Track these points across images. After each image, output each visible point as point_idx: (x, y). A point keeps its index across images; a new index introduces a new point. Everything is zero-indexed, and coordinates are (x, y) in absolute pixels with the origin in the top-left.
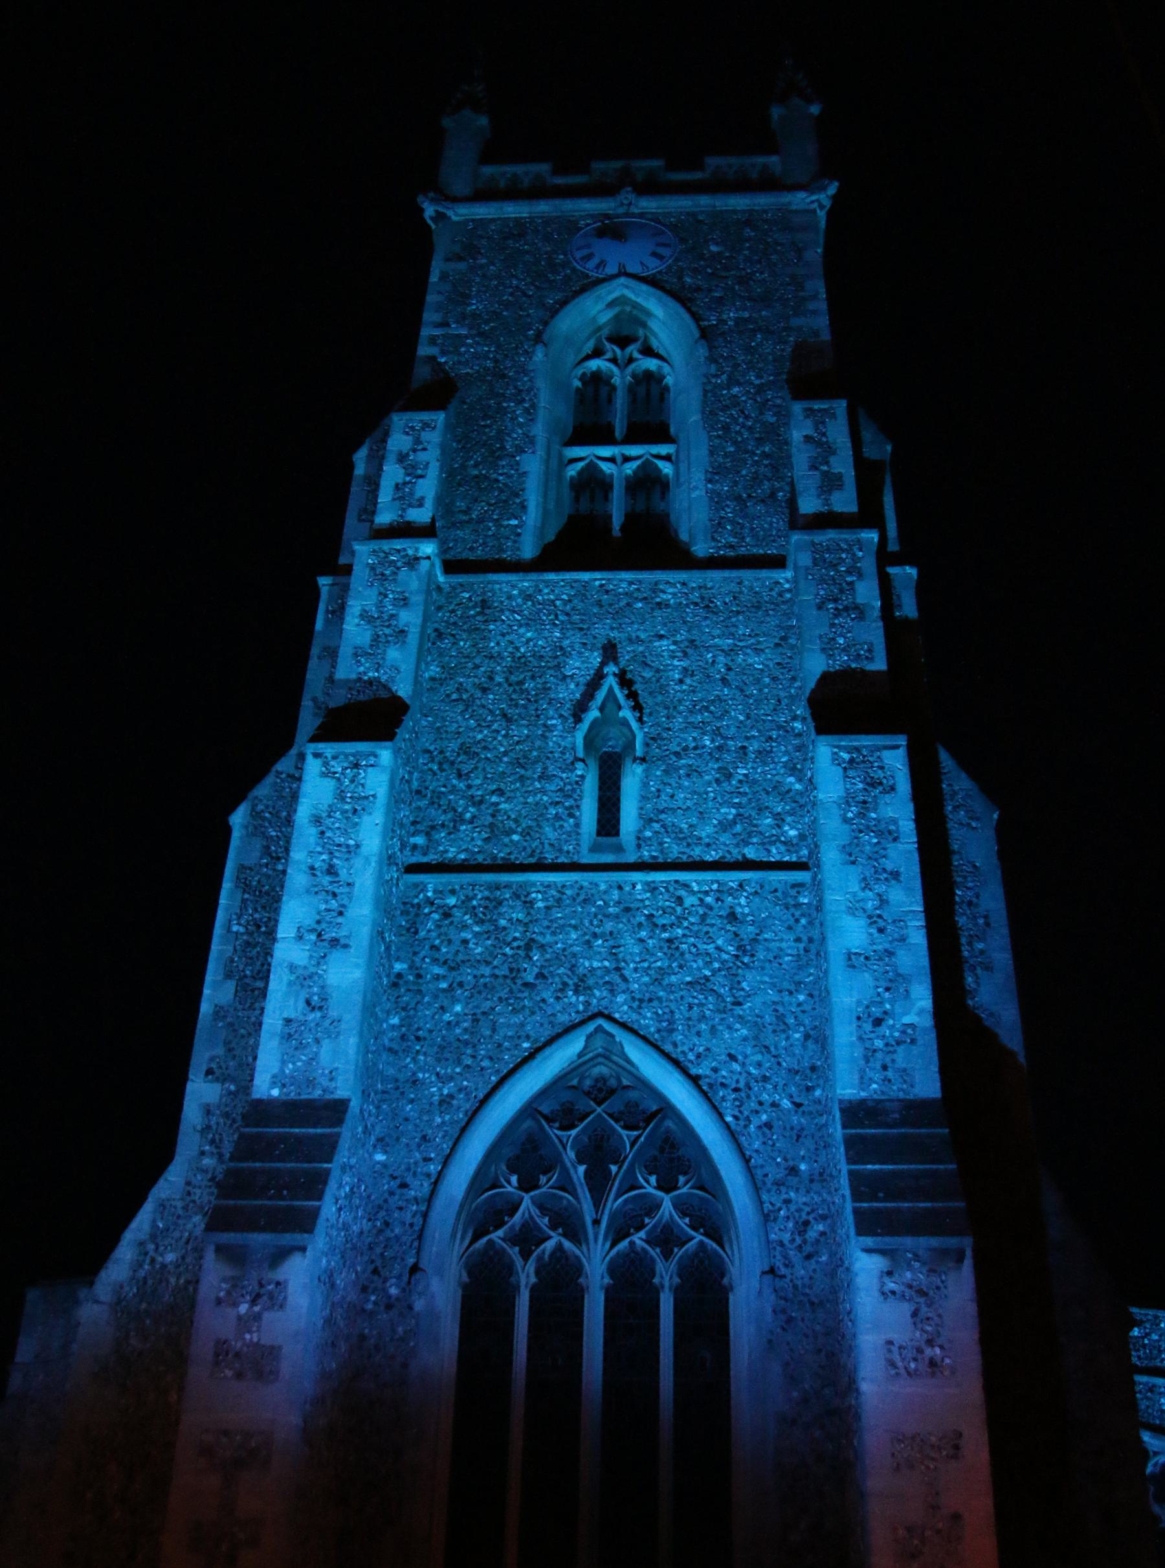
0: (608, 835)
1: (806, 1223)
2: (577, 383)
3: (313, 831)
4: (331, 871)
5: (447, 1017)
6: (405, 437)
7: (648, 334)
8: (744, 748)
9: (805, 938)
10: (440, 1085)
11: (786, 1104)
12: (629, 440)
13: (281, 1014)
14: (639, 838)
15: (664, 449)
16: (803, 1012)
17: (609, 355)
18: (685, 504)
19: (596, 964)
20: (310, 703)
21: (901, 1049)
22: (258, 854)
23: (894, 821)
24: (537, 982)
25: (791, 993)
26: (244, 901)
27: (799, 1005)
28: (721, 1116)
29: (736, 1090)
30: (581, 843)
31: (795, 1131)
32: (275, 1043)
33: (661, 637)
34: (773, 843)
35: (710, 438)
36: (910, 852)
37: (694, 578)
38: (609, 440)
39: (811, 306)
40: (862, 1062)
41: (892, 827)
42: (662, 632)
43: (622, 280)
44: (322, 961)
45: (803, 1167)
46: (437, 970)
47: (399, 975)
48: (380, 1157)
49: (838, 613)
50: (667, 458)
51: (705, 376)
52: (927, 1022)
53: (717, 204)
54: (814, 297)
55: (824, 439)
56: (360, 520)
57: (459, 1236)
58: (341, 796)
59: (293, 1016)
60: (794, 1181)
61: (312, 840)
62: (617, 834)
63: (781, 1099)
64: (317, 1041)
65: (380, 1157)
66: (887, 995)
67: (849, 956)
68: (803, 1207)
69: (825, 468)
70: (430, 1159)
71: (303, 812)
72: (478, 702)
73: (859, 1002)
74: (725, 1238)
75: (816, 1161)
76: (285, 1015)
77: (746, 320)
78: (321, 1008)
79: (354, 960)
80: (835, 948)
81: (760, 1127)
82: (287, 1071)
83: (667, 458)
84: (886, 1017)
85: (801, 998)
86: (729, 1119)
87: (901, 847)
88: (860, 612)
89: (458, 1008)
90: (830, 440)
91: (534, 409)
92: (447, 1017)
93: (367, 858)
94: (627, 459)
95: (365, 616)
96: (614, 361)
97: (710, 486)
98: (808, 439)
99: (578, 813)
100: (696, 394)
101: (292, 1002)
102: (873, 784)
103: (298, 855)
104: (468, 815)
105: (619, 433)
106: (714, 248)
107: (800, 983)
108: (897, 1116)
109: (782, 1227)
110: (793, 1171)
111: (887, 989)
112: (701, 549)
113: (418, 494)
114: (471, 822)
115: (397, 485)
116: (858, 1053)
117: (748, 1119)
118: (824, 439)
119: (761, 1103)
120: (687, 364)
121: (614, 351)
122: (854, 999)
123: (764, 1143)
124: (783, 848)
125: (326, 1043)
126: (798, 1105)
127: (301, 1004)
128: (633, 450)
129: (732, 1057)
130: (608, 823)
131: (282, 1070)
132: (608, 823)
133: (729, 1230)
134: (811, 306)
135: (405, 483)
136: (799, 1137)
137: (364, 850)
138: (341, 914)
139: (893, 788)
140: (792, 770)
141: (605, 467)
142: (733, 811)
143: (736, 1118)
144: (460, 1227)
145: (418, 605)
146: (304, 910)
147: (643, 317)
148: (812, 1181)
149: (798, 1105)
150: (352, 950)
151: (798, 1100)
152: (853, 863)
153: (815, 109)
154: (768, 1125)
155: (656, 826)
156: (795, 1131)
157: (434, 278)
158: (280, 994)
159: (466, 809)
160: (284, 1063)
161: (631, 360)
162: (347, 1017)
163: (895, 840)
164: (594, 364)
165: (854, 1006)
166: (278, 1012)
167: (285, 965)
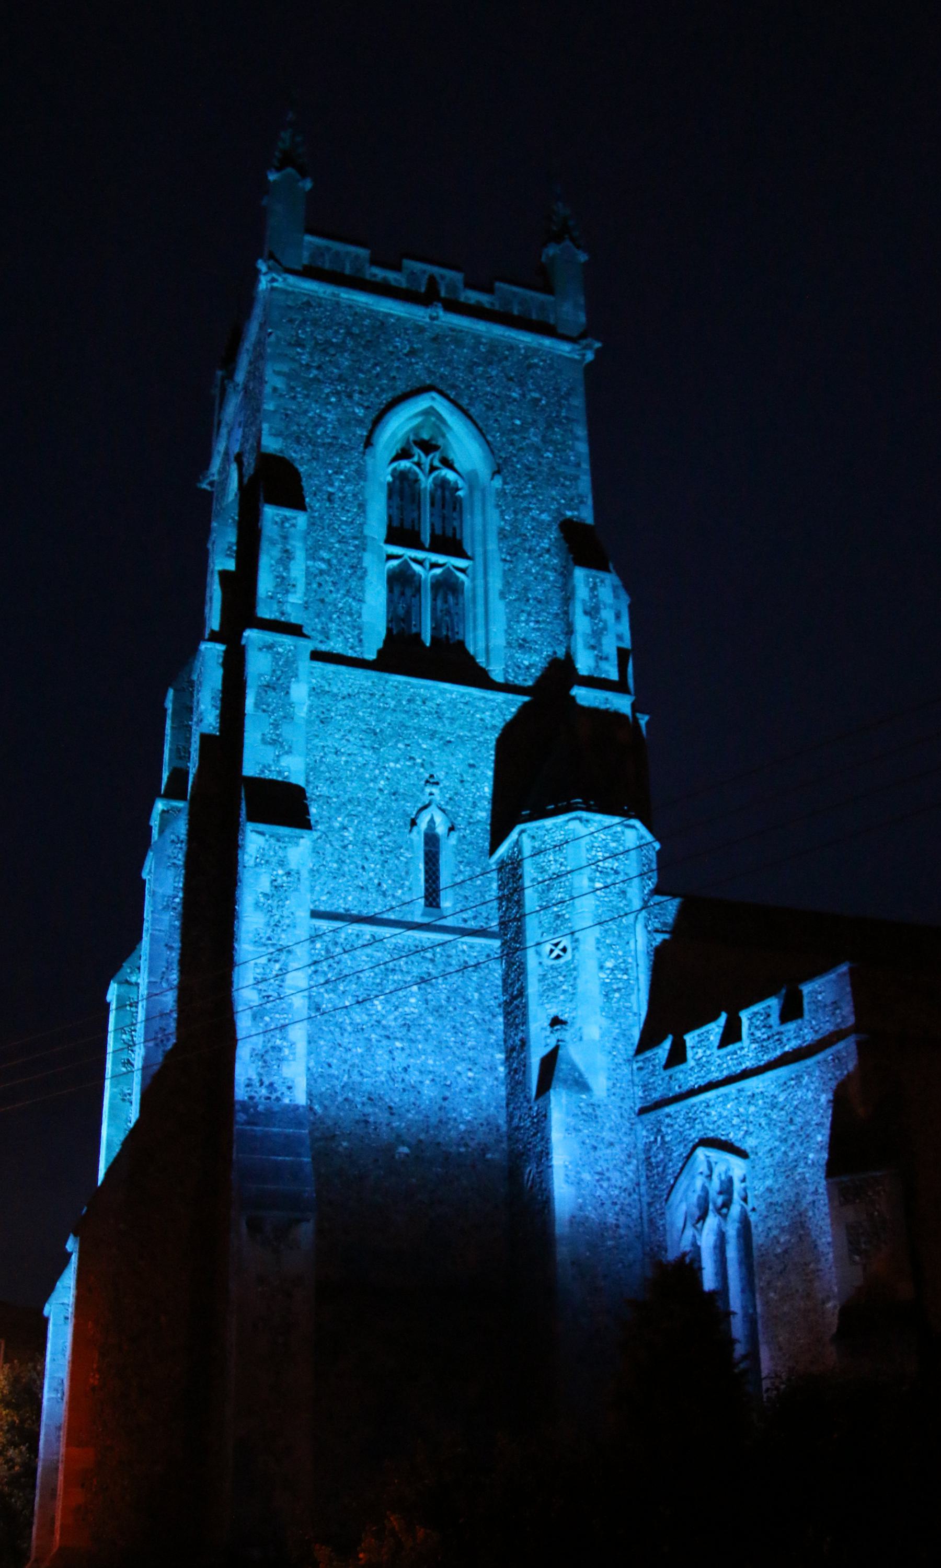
2: (390, 479)
12: (434, 549)
15: (461, 563)
17: (416, 459)
37: (489, 694)
38: (419, 546)
43: (434, 394)
50: (463, 571)
72: (371, 1131)
83: (463, 571)
94: (434, 565)
96: (418, 464)
105: (426, 538)
112: (497, 674)
121: (420, 457)
128: (441, 559)
130: (432, 897)
132: (432, 897)
141: (416, 568)
147: (444, 429)
153: (308, 185)
161: (433, 469)
164: (404, 464)
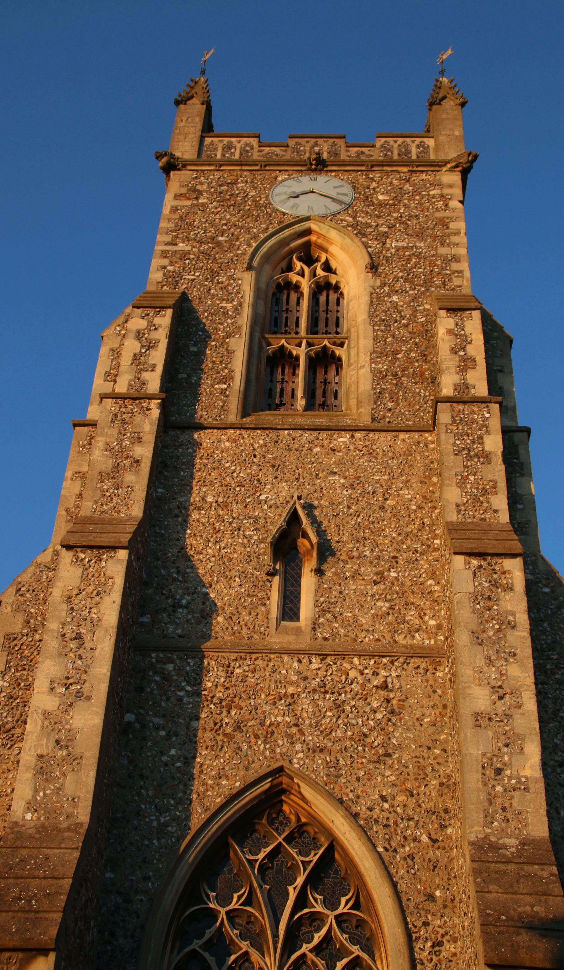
0: (291, 619)
1: (440, 944)
3: (65, 607)
4: (78, 637)
5: (165, 758)
6: (141, 321)
7: (329, 257)
8: (395, 557)
9: (440, 706)
10: (157, 814)
11: (425, 838)
13: (35, 752)
14: (314, 623)
16: (439, 764)
18: (354, 379)
19: (279, 719)
20: (64, 513)
21: (516, 794)
22: (20, 626)
23: (513, 613)
24: (235, 733)
25: (429, 748)
26: (8, 662)
27: (435, 758)
28: (374, 846)
29: (386, 826)
30: (270, 626)
31: (432, 863)
32: (29, 775)
33: (335, 473)
34: (417, 631)
35: (374, 330)
36: (524, 637)
39: (454, 239)
40: (486, 804)
41: (510, 618)
42: (335, 470)
44: (69, 709)
45: (438, 893)
46: (157, 720)
47: (129, 723)
48: (109, 875)
49: (469, 457)
51: (373, 287)
52: (538, 773)
53: (347, 835)
54: (457, 233)
55: (462, 332)
56: (106, 380)
57: (169, 946)
58: (85, 578)
59: (45, 752)
60: (430, 906)
61: (63, 614)
62: (298, 619)
63: (421, 834)
64: (64, 775)
65: (109, 875)
66: (505, 750)
67: (477, 716)
68: (438, 929)
69: (462, 353)
70: (149, 878)
71: (57, 593)
73: (484, 755)
74: (377, 956)
75: (448, 889)
76: (39, 752)
77: (404, 248)
78: (67, 747)
79: (95, 709)
80: (466, 711)
81: (405, 859)
82: (38, 798)
84: (505, 768)
85: (437, 752)
86: (381, 849)
87: (517, 633)
88: (487, 457)
89: (173, 752)
90: (467, 333)
91: (241, 306)
92: (165, 758)
93: (106, 630)
95: (108, 448)
97: (373, 365)
98: (450, 332)
99: (268, 602)
100: (365, 300)
101: (44, 742)
102: (495, 584)
103: (53, 625)
104: (184, 602)
106: (381, 197)
107: (436, 740)
108: (514, 850)
109: (422, 947)
110: (431, 898)
111: (507, 745)
113: (151, 361)
114: (187, 607)
115: (135, 355)
116: (483, 796)
117: (395, 851)
118: (462, 332)
119: (405, 838)
120: (358, 278)
122: (480, 752)
123: (408, 872)
124: (425, 636)
125: (70, 776)
126: (435, 841)
127: (52, 743)
129: (384, 799)
131: (34, 797)
133: (379, 949)
134: (454, 239)
135: (141, 354)
136: (435, 867)
137: (104, 622)
138: (86, 672)
139: (512, 589)
140: (433, 576)
142: (387, 605)
143: (386, 849)
144: (171, 938)
145: (149, 442)
146: (56, 668)
147: (326, 245)
148: (445, 907)
149: (435, 841)
150: (93, 701)
151: (434, 837)
152: (480, 644)
154: (411, 857)
155: (329, 616)
156: (432, 863)
157: (166, 210)
158: (35, 735)
159: (182, 597)
160: (36, 792)
162: (88, 754)
163: (513, 627)
165: (480, 758)
166: (33, 750)
167: (40, 711)
